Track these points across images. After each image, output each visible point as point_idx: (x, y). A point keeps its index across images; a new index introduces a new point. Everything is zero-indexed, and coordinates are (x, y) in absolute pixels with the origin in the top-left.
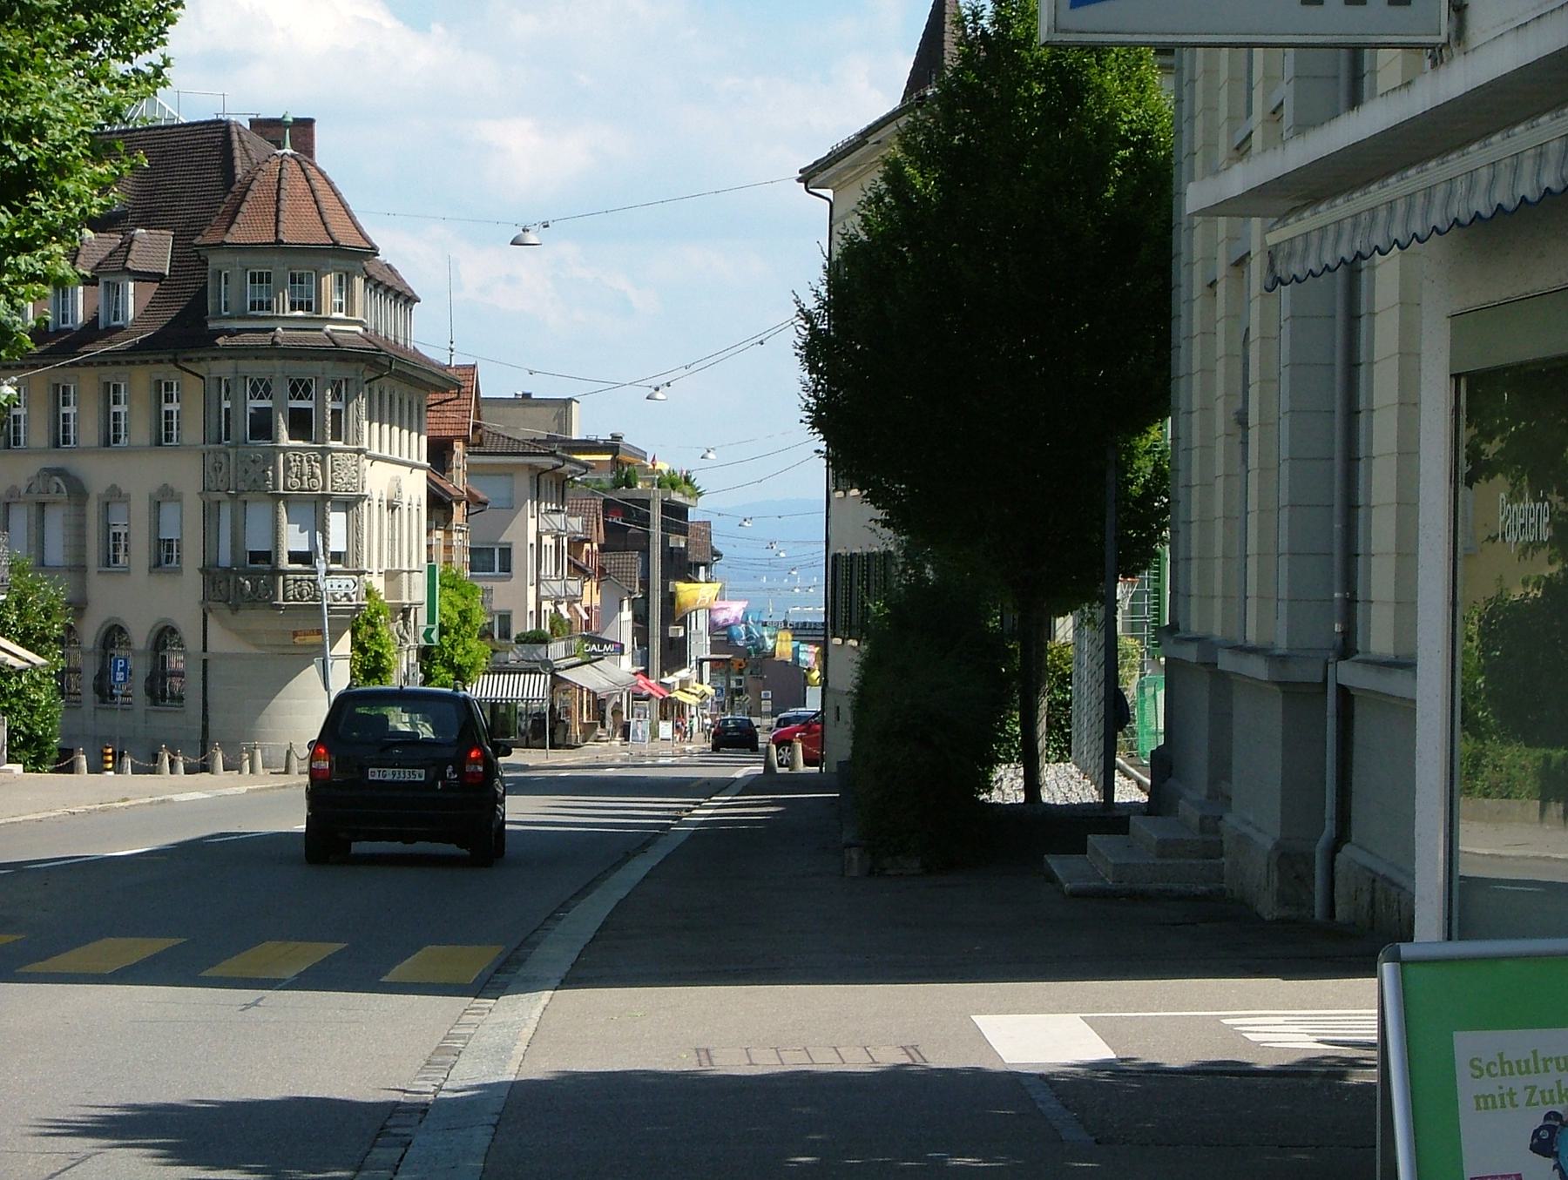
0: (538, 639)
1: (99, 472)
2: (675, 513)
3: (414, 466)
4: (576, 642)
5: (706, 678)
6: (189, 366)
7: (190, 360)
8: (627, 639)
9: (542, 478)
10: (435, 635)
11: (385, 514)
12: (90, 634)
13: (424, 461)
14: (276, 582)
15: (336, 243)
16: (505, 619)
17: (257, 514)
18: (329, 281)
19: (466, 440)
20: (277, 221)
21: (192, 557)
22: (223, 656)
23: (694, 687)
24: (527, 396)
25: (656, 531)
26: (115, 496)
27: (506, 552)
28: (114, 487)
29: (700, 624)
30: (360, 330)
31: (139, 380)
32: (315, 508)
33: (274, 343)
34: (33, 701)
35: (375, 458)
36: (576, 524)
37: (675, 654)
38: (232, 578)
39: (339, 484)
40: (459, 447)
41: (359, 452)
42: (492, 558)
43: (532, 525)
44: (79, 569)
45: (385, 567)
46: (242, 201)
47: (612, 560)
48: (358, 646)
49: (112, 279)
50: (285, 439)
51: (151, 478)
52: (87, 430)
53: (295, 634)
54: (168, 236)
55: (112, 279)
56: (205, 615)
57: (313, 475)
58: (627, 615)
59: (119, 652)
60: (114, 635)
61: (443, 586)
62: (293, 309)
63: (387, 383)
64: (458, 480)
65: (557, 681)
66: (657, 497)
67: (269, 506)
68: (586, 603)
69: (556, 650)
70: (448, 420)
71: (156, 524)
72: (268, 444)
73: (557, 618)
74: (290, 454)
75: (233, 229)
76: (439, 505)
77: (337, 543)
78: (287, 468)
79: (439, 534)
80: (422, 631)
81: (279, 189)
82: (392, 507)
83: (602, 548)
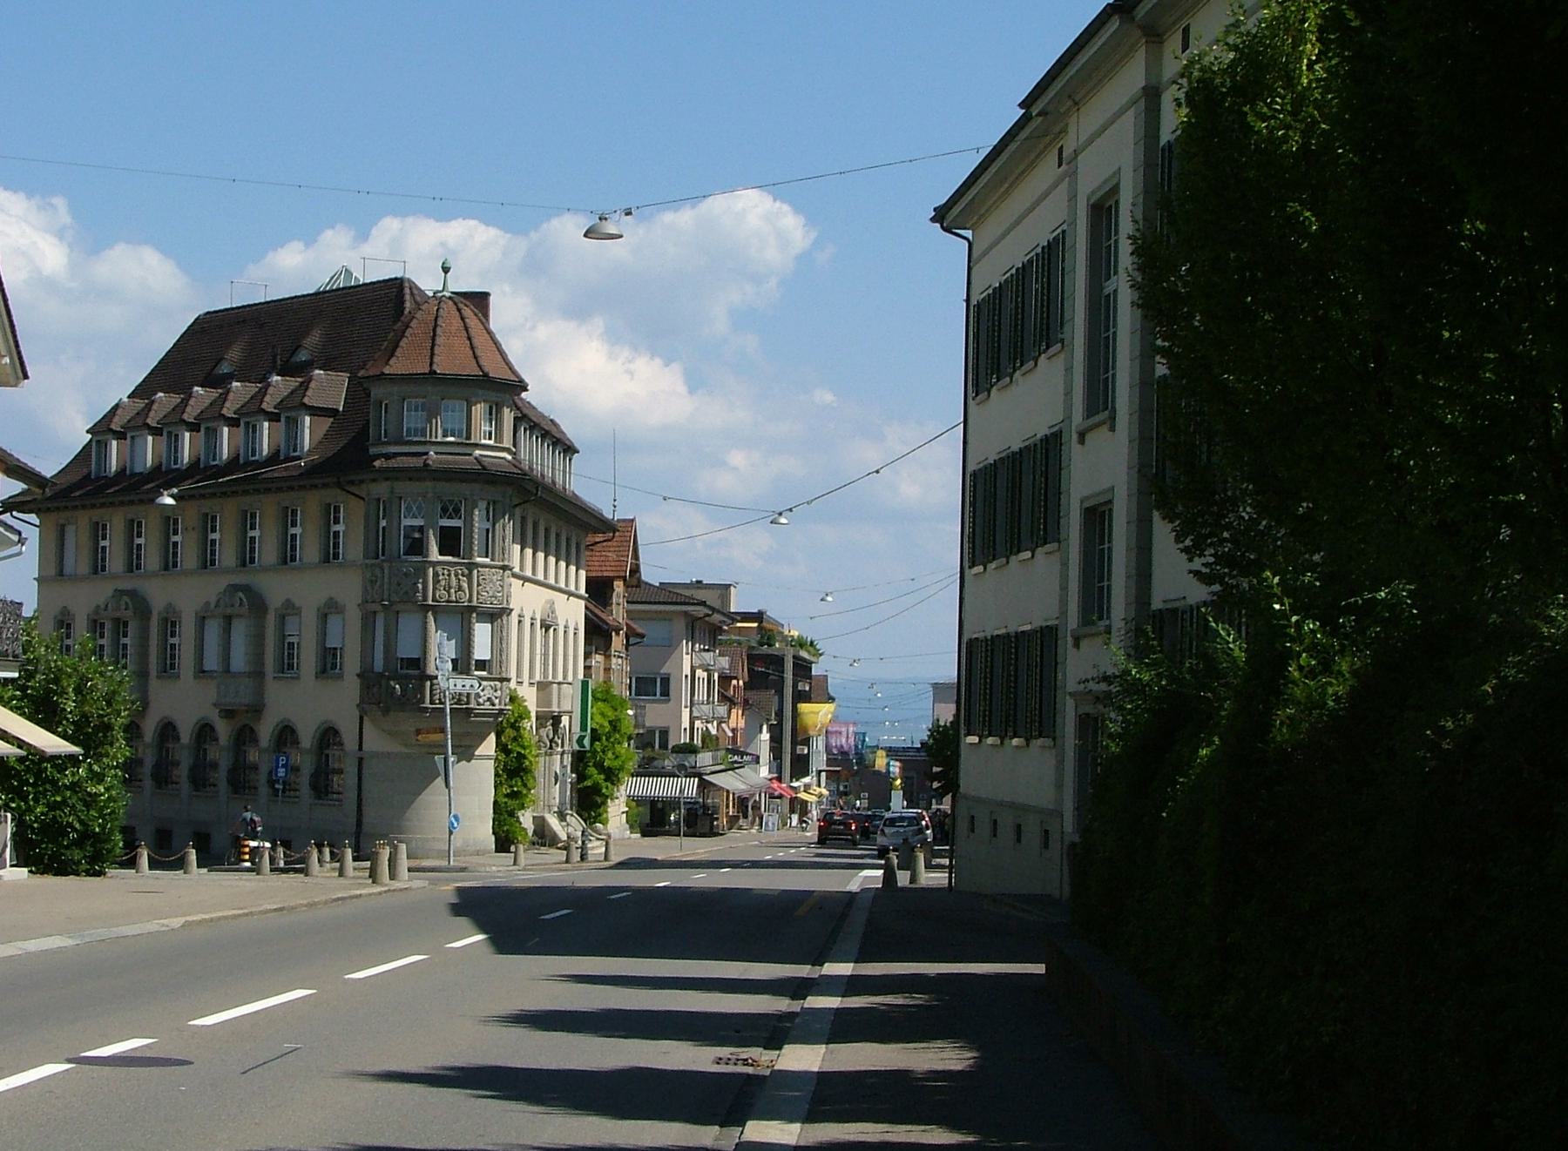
0: (690, 749)
1: (277, 588)
2: (803, 669)
3: (570, 594)
4: (721, 753)
5: (823, 784)
6: (352, 489)
7: (352, 483)
8: (765, 754)
9: (697, 625)
10: (586, 742)
11: (539, 632)
12: (149, 728)
13: (582, 591)
14: (422, 689)
15: (486, 375)
16: (664, 733)
17: (407, 625)
18: (479, 410)
19: (624, 579)
20: (432, 355)
21: (351, 663)
22: (376, 755)
23: (814, 790)
24: (699, 582)
25: (789, 675)
26: (290, 609)
27: (666, 681)
28: (288, 600)
29: (819, 744)
30: (509, 457)
31: (310, 504)
32: (461, 618)
33: (426, 465)
34: (90, 794)
35: (526, 580)
36: (724, 662)
37: (801, 766)
38: (383, 682)
39: (486, 597)
40: (619, 586)
41: (504, 568)
42: (652, 686)
43: (687, 660)
44: (258, 674)
45: (537, 678)
46: (403, 336)
47: (753, 696)
48: (502, 747)
49: (293, 414)
50: (434, 554)
51: (318, 594)
52: (268, 552)
53: (418, 732)
54: (344, 378)
55: (293, 414)
56: (361, 718)
57: (460, 588)
58: (765, 736)
59: (333, 752)
60: (168, 730)
61: (595, 699)
62: (445, 436)
63: (531, 512)
64: (618, 612)
65: (704, 786)
67: (419, 616)
68: (732, 724)
69: (704, 759)
70: (607, 560)
71: (323, 634)
72: (419, 559)
73: (706, 735)
74: (439, 569)
75: (392, 362)
76: (597, 634)
77: (481, 651)
78: (436, 581)
79: (598, 659)
80: (576, 737)
81: (436, 326)
82: (546, 627)
83: (748, 686)
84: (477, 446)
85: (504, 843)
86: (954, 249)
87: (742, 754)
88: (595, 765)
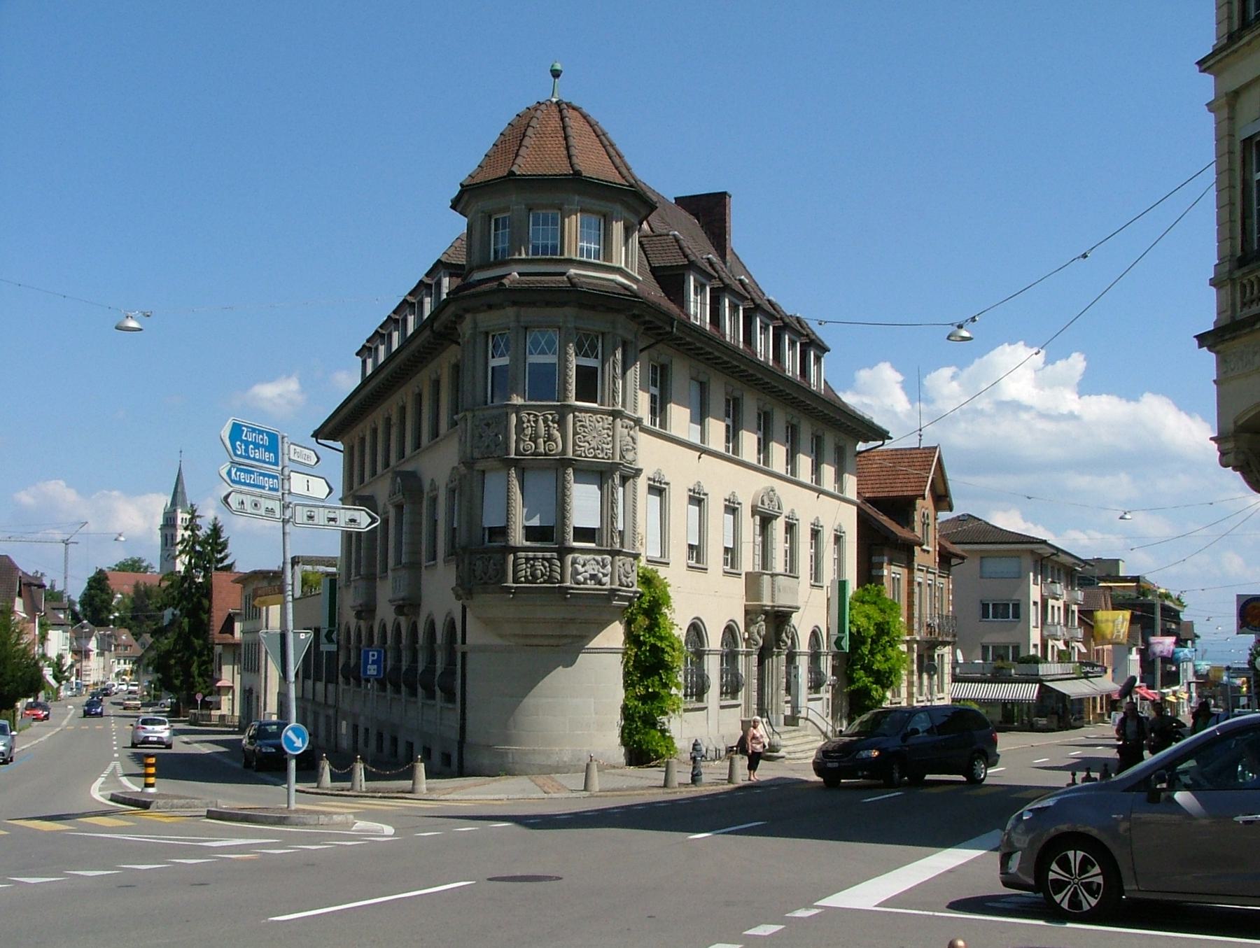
13: (854, 497)
14: (505, 561)
15: (577, 173)
16: (1016, 648)
22: (482, 649)
27: (1017, 606)
41: (616, 414)
48: (632, 638)
57: (550, 438)
63: (664, 353)
66: (1158, 602)
67: (548, 479)
80: (833, 639)
84: (570, 262)
85: (639, 755)
86: (1209, 79)
87: (1093, 665)
88: (864, 668)
